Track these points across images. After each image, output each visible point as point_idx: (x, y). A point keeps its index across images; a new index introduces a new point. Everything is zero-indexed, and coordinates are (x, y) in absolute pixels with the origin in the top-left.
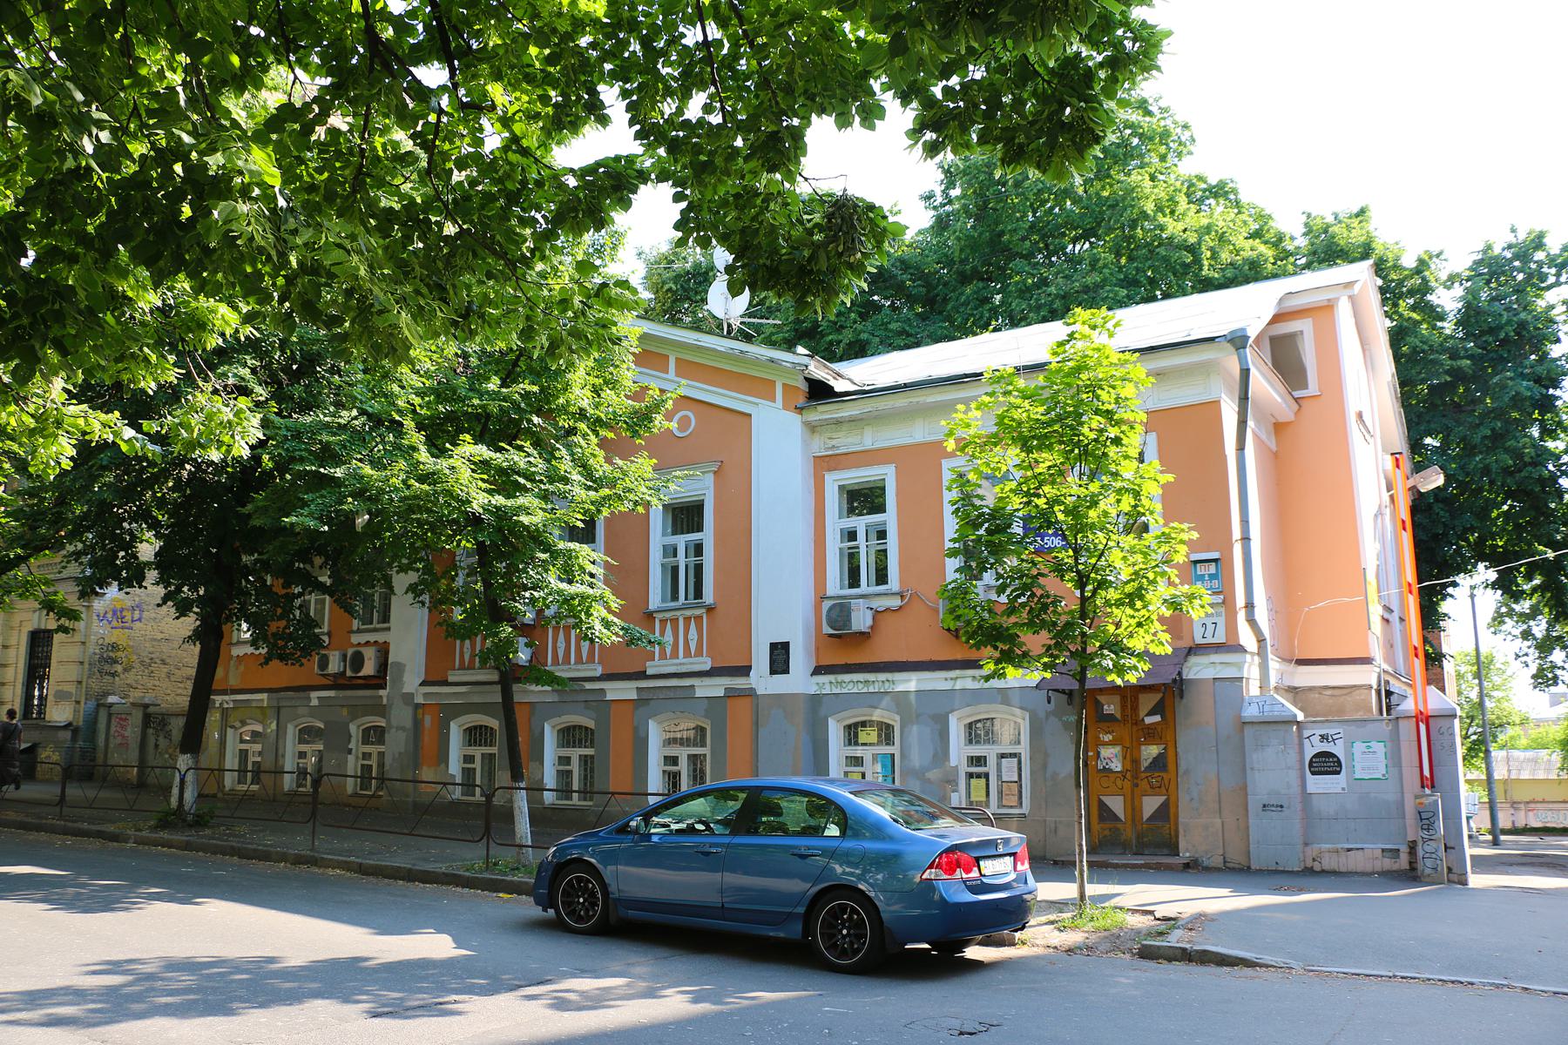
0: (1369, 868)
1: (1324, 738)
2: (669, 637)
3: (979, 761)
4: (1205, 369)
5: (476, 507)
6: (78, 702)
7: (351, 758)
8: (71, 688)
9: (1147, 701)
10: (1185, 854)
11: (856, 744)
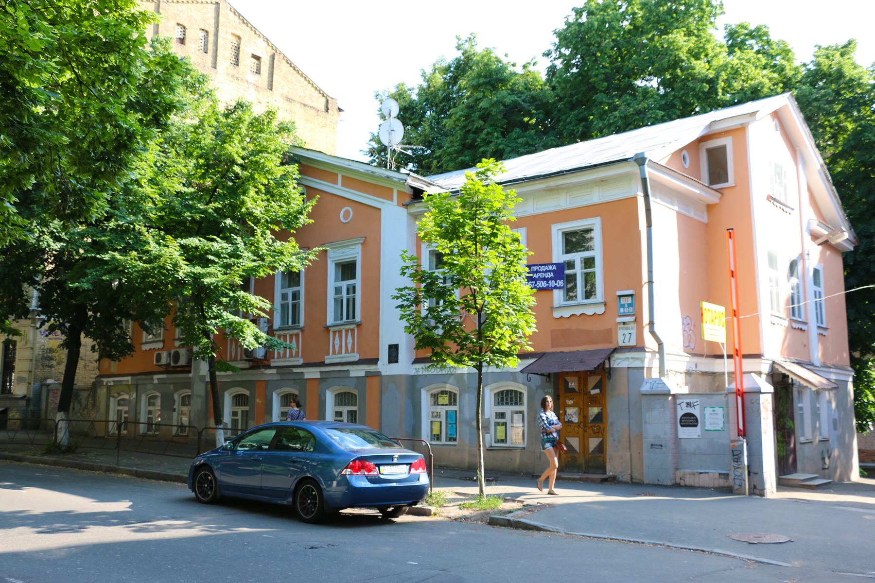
0: (711, 485)
1: (688, 404)
2: (294, 345)
3: (502, 415)
4: (627, 177)
5: (181, 275)
6: (29, 383)
7: (175, 414)
8: (25, 375)
9: (593, 381)
10: (610, 473)
11: (438, 405)
